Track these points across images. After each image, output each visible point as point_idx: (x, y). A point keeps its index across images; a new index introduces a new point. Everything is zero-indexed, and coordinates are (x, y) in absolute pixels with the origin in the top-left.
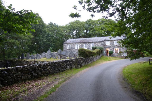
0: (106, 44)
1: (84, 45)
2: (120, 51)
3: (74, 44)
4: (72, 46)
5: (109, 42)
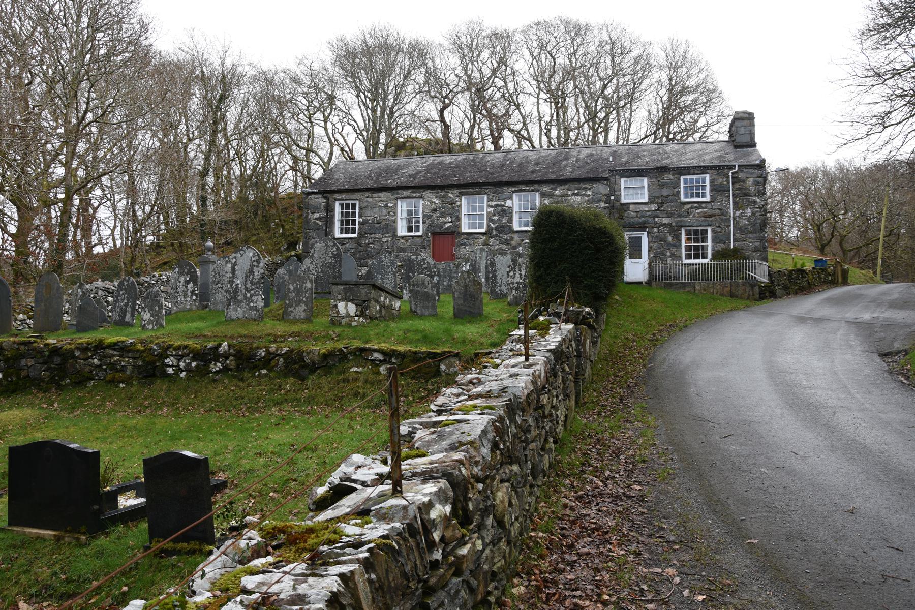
0: (623, 201)
1: (465, 205)
2: (720, 247)
3: (383, 195)
4: (373, 214)
5: (646, 180)
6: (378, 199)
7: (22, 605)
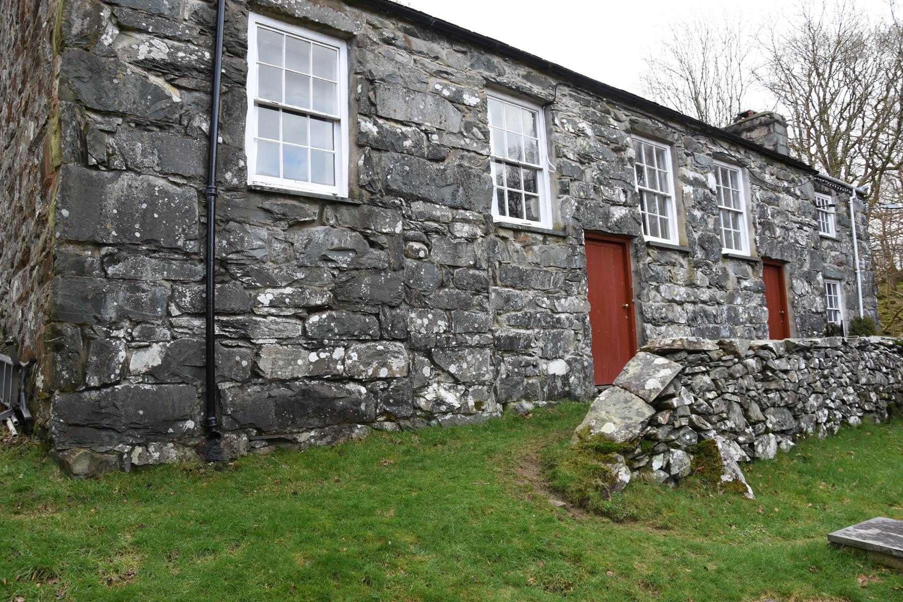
6: (434, 66)
7: (804, 600)
